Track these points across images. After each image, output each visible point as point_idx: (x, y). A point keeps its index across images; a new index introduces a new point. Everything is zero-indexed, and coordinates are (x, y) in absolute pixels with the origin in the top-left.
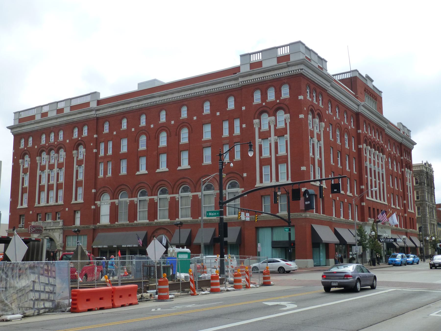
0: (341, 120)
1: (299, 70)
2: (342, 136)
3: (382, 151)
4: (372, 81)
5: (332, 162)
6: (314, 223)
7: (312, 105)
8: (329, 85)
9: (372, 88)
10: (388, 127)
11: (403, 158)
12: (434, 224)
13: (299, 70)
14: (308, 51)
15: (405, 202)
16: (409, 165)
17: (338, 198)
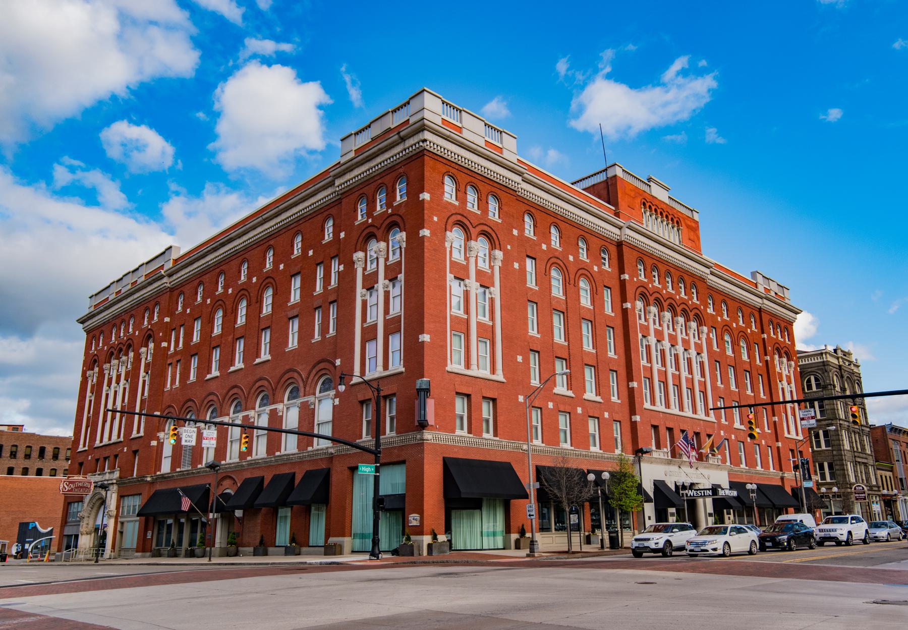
0: (746, 328)
2: (735, 345)
5: (762, 394)
7: (777, 342)
8: (518, 179)
10: (712, 273)
12: (865, 464)
15: (776, 419)
16: (788, 352)
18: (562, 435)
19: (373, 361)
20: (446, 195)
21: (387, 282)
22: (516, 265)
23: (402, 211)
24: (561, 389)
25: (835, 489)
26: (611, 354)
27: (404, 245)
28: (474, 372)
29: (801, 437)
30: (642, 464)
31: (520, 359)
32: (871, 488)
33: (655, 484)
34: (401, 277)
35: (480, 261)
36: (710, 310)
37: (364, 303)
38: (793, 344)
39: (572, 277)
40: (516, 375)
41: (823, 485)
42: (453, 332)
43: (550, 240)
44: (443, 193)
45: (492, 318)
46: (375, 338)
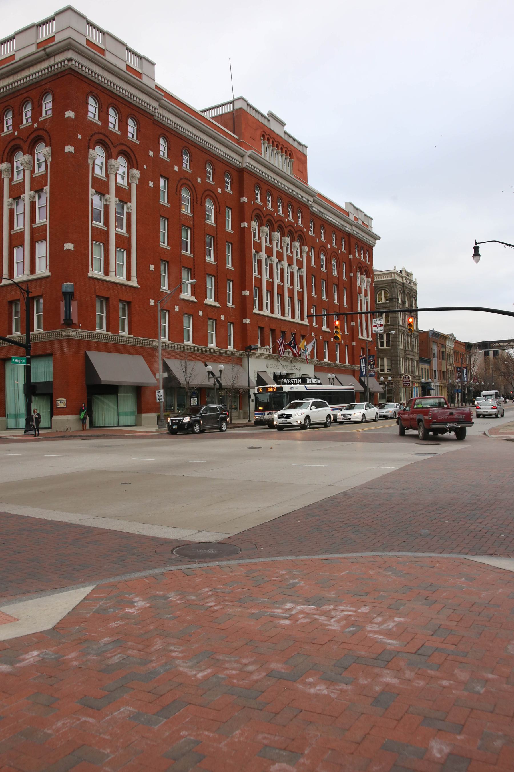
1: (66, 62)
2: (328, 262)
3: (303, 240)
4: (283, 124)
5: (345, 304)
6: (90, 350)
7: (360, 262)
8: (156, 104)
9: (282, 135)
10: (315, 202)
11: (351, 256)
12: (412, 360)
13: (66, 62)
14: (367, 218)
15: (353, 324)
16: (367, 270)
17: (321, 337)
18: (184, 246)
19: (21, 266)
20: (90, 115)
21: (32, 193)
22: (151, 184)
23: (48, 126)
24: (186, 295)
25: (390, 378)
26: (229, 266)
27: (50, 159)
28: (112, 278)
29: (370, 339)
30: (250, 359)
31: (152, 267)
32: (414, 377)
33: (258, 375)
34: (47, 189)
35: (119, 177)
36: (311, 233)
37: (11, 212)
38: (372, 265)
39: (199, 197)
40: (149, 281)
41: (382, 375)
42: (94, 242)
43: (182, 163)
44: (87, 111)
45: (129, 230)
46: (22, 244)
